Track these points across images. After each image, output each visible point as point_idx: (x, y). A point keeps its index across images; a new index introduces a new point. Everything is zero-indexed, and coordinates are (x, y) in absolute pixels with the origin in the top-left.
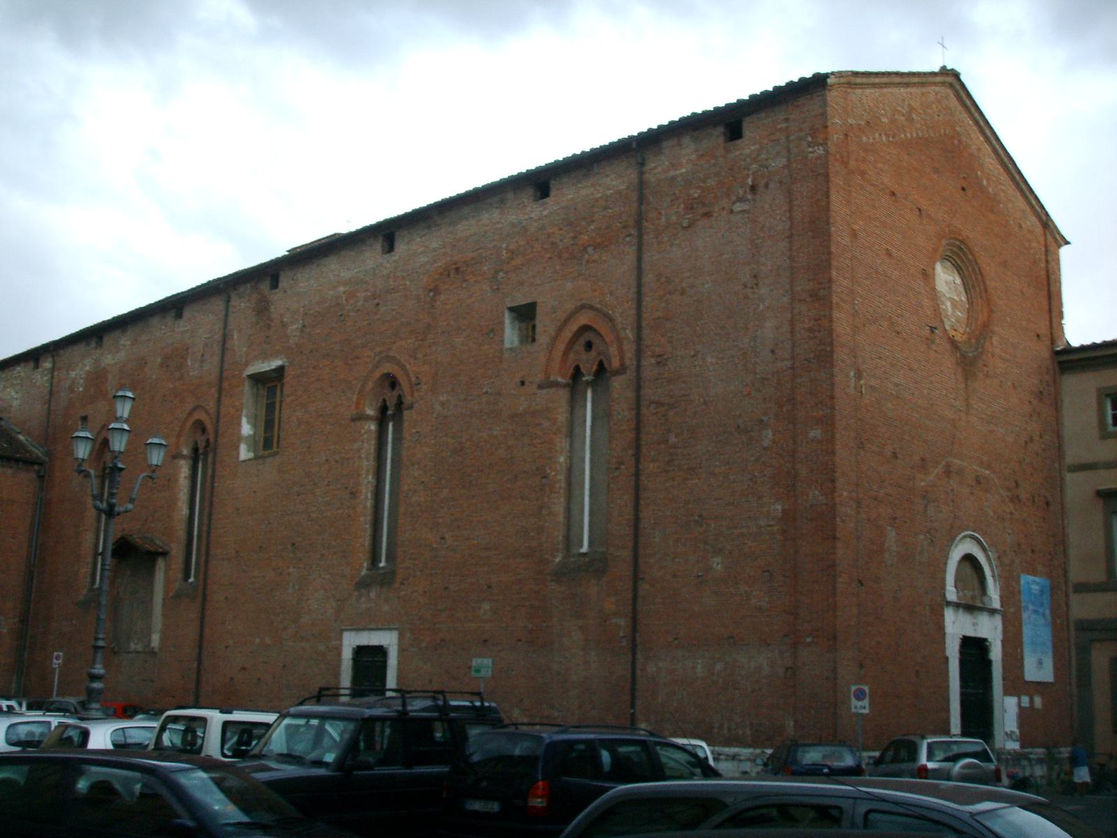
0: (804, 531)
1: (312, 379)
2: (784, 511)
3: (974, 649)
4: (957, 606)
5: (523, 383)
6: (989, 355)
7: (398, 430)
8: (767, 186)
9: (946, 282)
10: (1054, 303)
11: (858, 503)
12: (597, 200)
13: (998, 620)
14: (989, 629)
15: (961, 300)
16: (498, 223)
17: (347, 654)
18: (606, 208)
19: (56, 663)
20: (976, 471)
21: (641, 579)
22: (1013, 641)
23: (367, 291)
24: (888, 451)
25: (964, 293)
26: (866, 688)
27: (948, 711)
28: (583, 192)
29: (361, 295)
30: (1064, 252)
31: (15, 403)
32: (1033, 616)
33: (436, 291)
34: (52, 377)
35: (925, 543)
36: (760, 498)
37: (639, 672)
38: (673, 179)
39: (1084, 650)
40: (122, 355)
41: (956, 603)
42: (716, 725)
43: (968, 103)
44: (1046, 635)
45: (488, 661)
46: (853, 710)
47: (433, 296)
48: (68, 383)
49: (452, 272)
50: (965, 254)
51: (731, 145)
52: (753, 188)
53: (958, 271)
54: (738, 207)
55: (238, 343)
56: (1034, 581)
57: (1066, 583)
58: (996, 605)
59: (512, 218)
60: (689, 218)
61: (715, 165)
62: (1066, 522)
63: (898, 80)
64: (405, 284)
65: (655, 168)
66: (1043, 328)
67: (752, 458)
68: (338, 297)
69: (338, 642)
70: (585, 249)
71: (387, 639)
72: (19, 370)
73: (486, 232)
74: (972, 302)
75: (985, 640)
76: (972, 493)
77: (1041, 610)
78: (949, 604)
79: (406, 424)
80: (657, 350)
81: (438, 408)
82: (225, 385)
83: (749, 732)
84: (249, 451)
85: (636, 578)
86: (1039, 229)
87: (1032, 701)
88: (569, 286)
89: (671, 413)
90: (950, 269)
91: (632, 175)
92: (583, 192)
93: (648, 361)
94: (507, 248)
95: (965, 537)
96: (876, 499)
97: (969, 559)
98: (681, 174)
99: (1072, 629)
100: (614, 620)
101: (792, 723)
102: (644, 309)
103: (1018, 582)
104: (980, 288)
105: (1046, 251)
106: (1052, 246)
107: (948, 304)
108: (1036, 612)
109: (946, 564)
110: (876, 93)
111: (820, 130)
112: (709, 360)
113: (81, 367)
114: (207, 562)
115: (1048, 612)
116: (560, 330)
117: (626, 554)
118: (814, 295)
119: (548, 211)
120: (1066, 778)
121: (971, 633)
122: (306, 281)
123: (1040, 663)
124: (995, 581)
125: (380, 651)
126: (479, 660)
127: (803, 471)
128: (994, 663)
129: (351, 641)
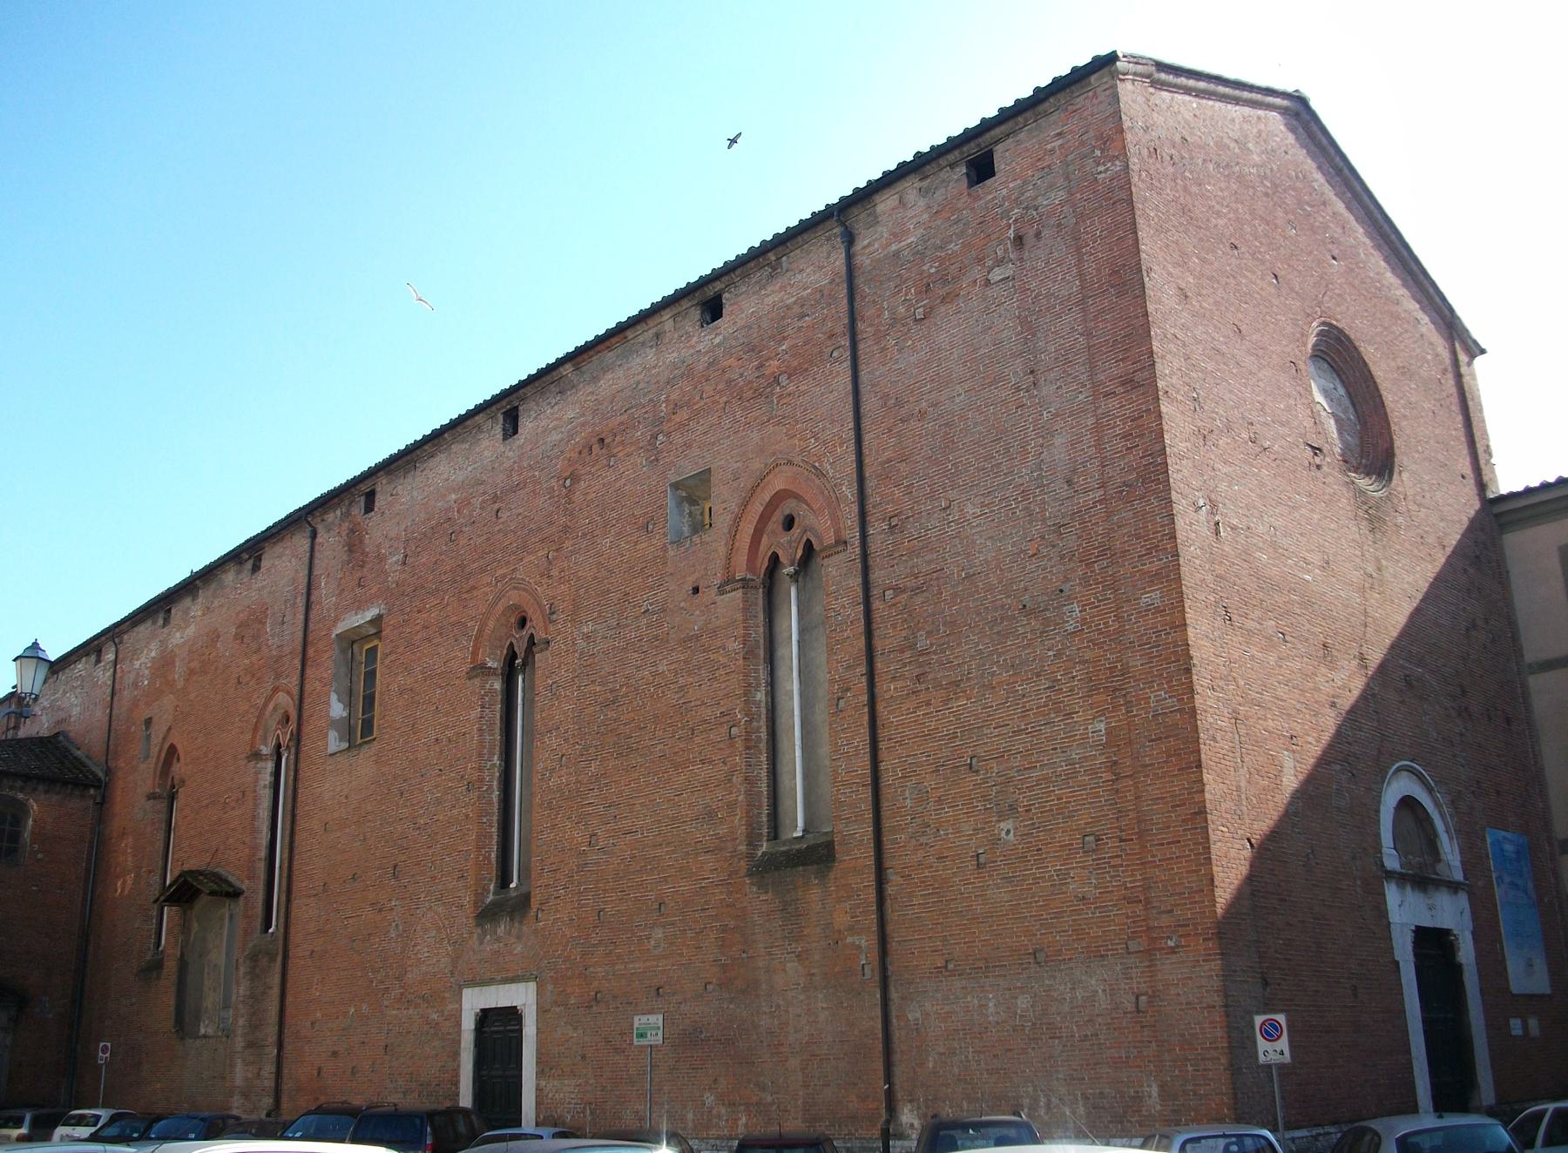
1: (418, 628)
2: (1109, 732)
3: (1432, 943)
4: (1401, 879)
5: (696, 590)
7: (530, 688)
8: (1038, 235)
12: (789, 308)
13: (1463, 900)
14: (1450, 913)
16: (654, 367)
17: (468, 1024)
18: (802, 316)
19: (103, 1057)
20: (1402, 667)
22: (1486, 930)
23: (485, 493)
25: (1351, 410)
27: (1408, 1051)
28: (769, 300)
29: (477, 502)
31: (75, 711)
33: (575, 478)
34: (115, 672)
35: (1343, 777)
38: (897, 254)
40: (191, 631)
41: (1400, 874)
43: (1325, 141)
45: (656, 1019)
46: (1262, 1059)
47: (571, 485)
48: (132, 676)
49: (596, 448)
51: (978, 189)
52: (1019, 240)
54: (996, 275)
55: (326, 592)
56: (1504, 838)
58: (1458, 876)
59: (672, 357)
60: (924, 306)
61: (958, 221)
64: (534, 476)
65: (869, 245)
67: (1051, 653)
68: (449, 509)
71: (521, 996)
72: (80, 667)
73: (638, 383)
75: (1447, 932)
76: (1403, 702)
78: (1390, 875)
79: (539, 673)
80: (890, 508)
81: (581, 643)
82: (311, 652)
84: (341, 741)
87: (1525, 1026)
88: (755, 436)
89: (919, 600)
91: (839, 260)
92: (769, 300)
93: (876, 528)
94: (667, 400)
95: (1399, 770)
98: (909, 245)
100: (849, 940)
101: (1155, 1091)
102: (866, 451)
104: (1374, 402)
106: (1463, 358)
108: (1513, 885)
109: (1378, 811)
110: (1194, 102)
111: (1112, 136)
112: (970, 509)
113: (145, 652)
114: (288, 901)
115: (1530, 885)
116: (745, 505)
117: (866, 831)
118: (1129, 383)
119: (721, 337)
122: (405, 495)
123: (1530, 965)
124: (1451, 839)
125: (512, 1015)
126: (644, 1019)
127: (1136, 662)
129: (475, 1001)
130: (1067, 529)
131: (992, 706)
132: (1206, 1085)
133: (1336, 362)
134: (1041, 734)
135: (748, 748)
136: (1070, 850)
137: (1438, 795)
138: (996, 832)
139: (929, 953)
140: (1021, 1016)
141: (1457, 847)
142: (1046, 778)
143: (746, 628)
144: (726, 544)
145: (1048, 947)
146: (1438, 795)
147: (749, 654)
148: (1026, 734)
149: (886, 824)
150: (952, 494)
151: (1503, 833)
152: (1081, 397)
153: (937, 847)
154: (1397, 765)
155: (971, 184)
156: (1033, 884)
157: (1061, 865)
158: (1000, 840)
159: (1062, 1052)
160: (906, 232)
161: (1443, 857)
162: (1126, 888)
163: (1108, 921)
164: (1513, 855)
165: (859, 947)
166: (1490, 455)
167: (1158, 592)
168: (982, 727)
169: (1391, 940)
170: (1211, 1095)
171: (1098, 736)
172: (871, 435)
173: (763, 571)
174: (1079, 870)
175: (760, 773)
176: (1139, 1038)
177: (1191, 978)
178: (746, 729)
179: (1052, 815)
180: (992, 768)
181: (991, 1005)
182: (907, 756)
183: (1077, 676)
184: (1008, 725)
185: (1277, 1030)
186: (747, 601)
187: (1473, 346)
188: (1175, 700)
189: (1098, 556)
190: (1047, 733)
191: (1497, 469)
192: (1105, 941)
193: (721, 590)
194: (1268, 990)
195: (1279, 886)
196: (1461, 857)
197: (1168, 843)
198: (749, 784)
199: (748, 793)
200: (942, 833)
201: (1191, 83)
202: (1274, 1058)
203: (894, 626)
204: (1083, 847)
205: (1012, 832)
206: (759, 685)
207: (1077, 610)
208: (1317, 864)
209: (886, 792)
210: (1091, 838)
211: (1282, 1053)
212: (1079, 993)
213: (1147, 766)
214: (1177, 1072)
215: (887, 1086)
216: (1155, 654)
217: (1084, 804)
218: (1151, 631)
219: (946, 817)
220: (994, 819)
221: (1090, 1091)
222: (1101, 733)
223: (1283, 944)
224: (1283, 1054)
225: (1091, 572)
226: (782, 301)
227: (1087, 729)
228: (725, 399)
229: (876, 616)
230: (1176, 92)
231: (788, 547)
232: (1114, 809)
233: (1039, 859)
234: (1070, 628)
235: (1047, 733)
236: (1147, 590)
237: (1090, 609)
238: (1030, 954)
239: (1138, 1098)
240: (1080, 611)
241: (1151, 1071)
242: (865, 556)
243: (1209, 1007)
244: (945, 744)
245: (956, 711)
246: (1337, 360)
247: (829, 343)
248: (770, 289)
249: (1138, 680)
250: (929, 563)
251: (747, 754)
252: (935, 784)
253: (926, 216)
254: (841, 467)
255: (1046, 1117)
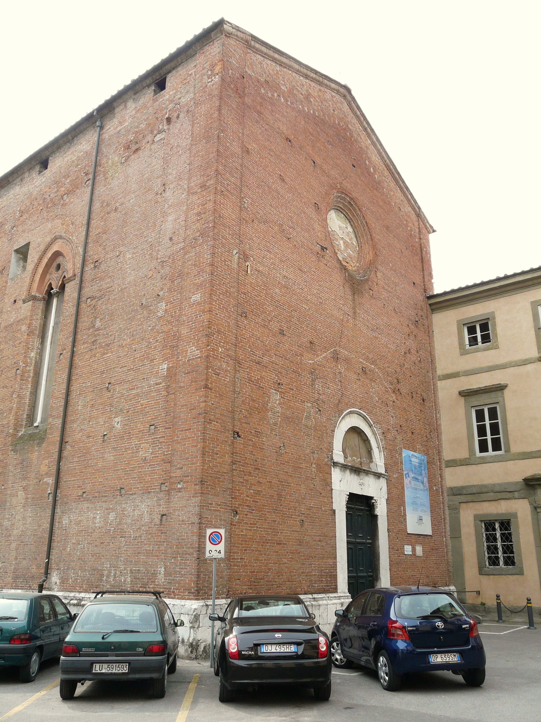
0: (182, 385)
2: (168, 369)
4: (344, 467)
5: (15, 301)
6: (375, 284)
8: (178, 117)
9: (340, 227)
10: (426, 267)
11: (238, 362)
13: (383, 482)
15: (352, 243)
21: (66, 442)
24: (275, 326)
25: (355, 239)
26: (222, 531)
28: (66, 159)
30: (432, 237)
32: (413, 482)
36: (152, 361)
37: (56, 524)
39: (455, 510)
42: (106, 573)
44: (424, 498)
46: (207, 555)
50: (355, 210)
53: (350, 222)
56: (413, 455)
57: (440, 459)
58: (382, 470)
62: (438, 415)
63: (297, 66)
66: (418, 280)
67: (150, 328)
69: (330, 561)
70: (62, 197)
74: (361, 246)
75: (372, 498)
77: (420, 478)
78: (335, 464)
83: (129, 579)
85: (62, 442)
86: (414, 217)
87: (414, 550)
90: (344, 219)
93: (89, 267)
96: (258, 363)
97: (355, 430)
99: (445, 494)
100: (45, 480)
103: (401, 454)
105: (420, 232)
106: (424, 231)
107: (341, 242)
115: (425, 480)
120: (356, 644)
121: (358, 491)
124: (380, 452)
127: (184, 331)
128: (379, 517)
130: (166, 263)
131: (121, 357)
132: (185, 568)
133: (348, 215)
134: (139, 371)
135: (22, 380)
136: (143, 433)
137: (375, 429)
138: (113, 423)
139: (76, 488)
140: (110, 524)
141: (383, 455)
142: (138, 395)
143: (31, 320)
144: (30, 279)
145: (127, 486)
146: (375, 429)
147: (30, 333)
148: (133, 371)
149: (69, 418)
150: (122, 249)
151: (412, 453)
152: (183, 196)
153: (88, 431)
154: (350, 410)
155: (156, 93)
156: (124, 451)
157: (138, 442)
158: (114, 427)
159: (125, 545)
160: (125, 121)
161: (374, 460)
162: (164, 455)
163: (154, 473)
164: (417, 464)
165: (48, 484)
166: (432, 278)
167: (200, 294)
168: (115, 367)
169: (332, 498)
170: (187, 575)
171: (163, 372)
172: (94, 221)
173: (45, 292)
174: (145, 445)
175: (27, 393)
176: (159, 540)
177: (186, 507)
178: (22, 370)
179: (138, 414)
180: (116, 389)
181: (98, 517)
182: (83, 383)
183: (159, 340)
184: (126, 366)
185: (212, 538)
186: (34, 307)
187: (429, 228)
188: (199, 351)
189: (177, 277)
190: (142, 370)
191: (434, 285)
192: (151, 484)
193: (24, 302)
194: (238, 517)
195: (256, 461)
196: (385, 461)
197: (186, 430)
198: (20, 398)
199: (19, 403)
200: (91, 423)
201: (276, 56)
202: (215, 555)
203: (88, 316)
204: (149, 432)
205: (120, 423)
206: (33, 349)
207: (164, 305)
208: (286, 452)
209: (72, 402)
210: (153, 427)
211: (220, 552)
212: (136, 512)
213: (182, 387)
214: (173, 561)
215: (47, 560)
216: (194, 327)
217: (152, 408)
218: (194, 315)
219: (94, 415)
220: (113, 416)
221: (134, 568)
222: (165, 370)
223: (253, 493)
224: (220, 553)
225: (173, 285)
226: (71, 159)
227: (159, 368)
228: (41, 208)
229: (82, 312)
230: (266, 58)
231: (55, 279)
232: (165, 411)
233: (129, 438)
234: (159, 315)
235: (142, 370)
236: (195, 293)
237: (170, 304)
238: (118, 490)
239: (154, 574)
240: (165, 306)
241: (162, 559)
242: (81, 281)
243: (192, 523)
244: (99, 377)
245: (106, 359)
246: (349, 214)
247: (85, 178)
248: (67, 153)
249: (184, 341)
250: (107, 283)
251: (20, 383)
252: (92, 398)
253: (134, 112)
254: (79, 238)
255: (113, 582)
